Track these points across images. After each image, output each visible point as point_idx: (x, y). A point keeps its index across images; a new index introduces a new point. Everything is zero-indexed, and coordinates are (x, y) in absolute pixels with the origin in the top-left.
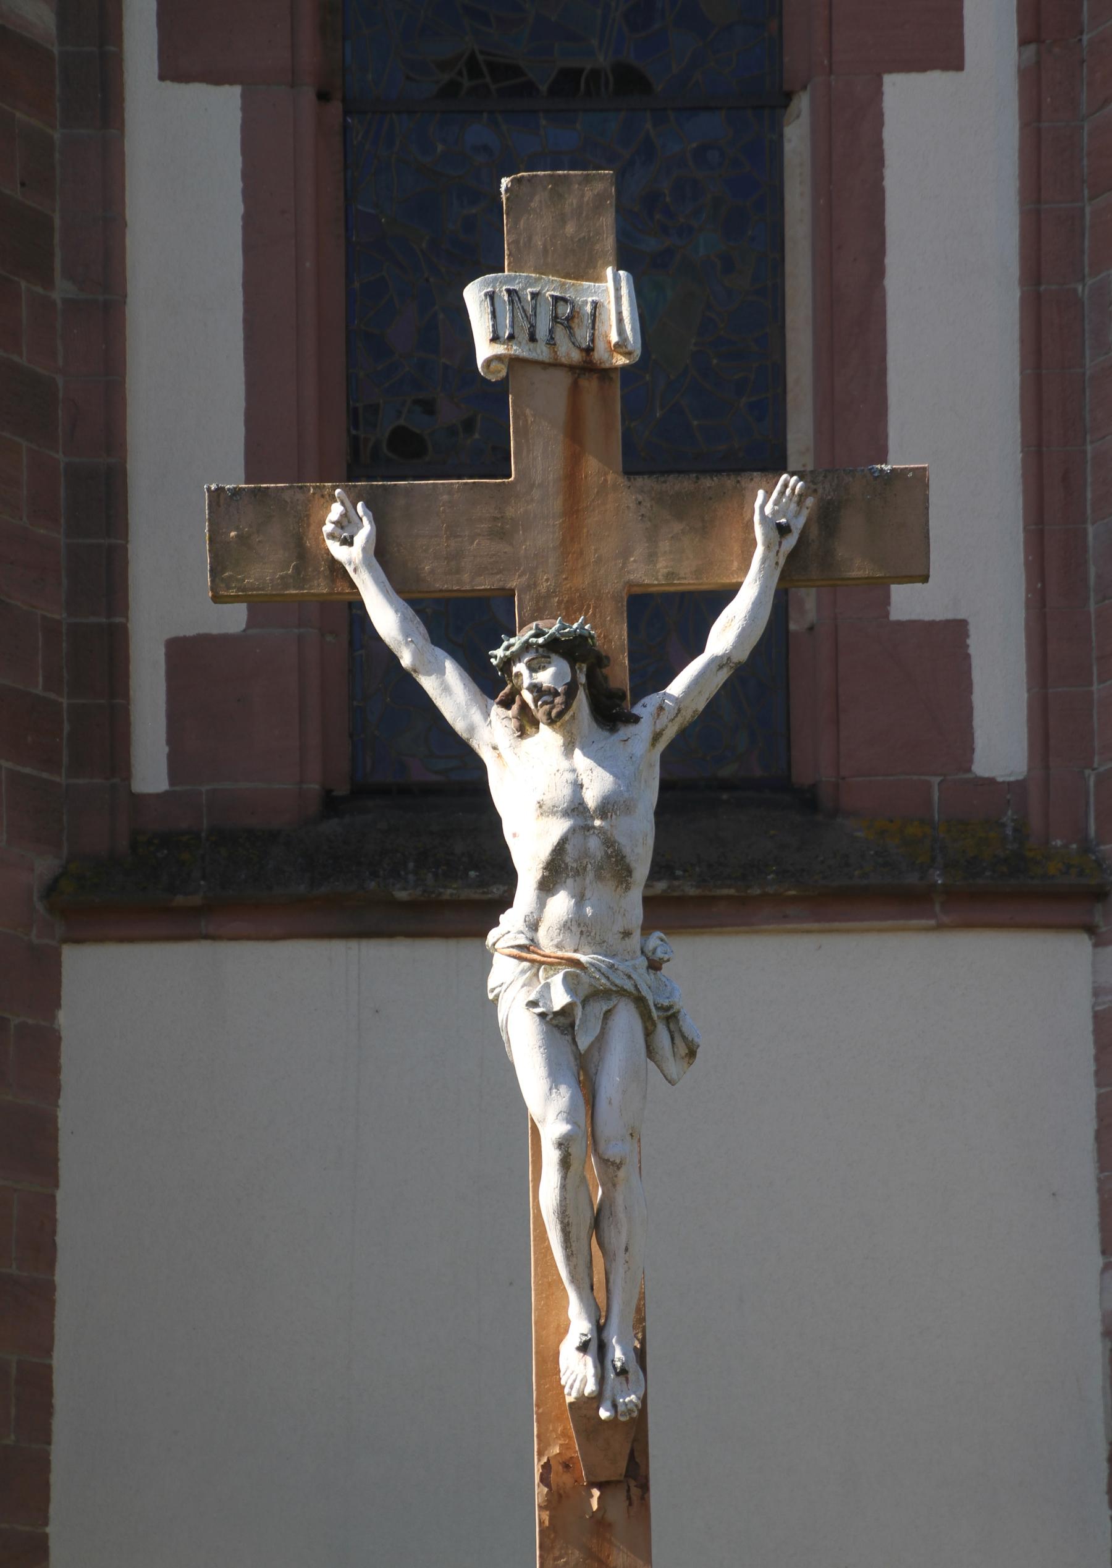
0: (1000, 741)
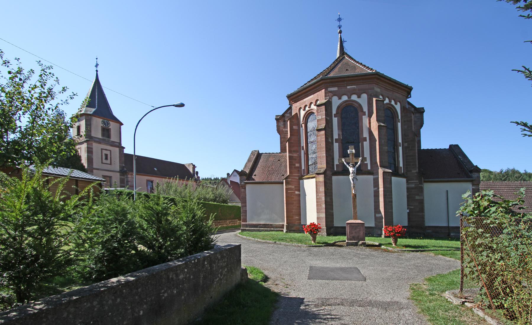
0: (369, 168)
